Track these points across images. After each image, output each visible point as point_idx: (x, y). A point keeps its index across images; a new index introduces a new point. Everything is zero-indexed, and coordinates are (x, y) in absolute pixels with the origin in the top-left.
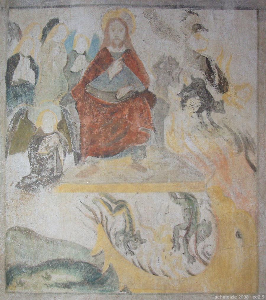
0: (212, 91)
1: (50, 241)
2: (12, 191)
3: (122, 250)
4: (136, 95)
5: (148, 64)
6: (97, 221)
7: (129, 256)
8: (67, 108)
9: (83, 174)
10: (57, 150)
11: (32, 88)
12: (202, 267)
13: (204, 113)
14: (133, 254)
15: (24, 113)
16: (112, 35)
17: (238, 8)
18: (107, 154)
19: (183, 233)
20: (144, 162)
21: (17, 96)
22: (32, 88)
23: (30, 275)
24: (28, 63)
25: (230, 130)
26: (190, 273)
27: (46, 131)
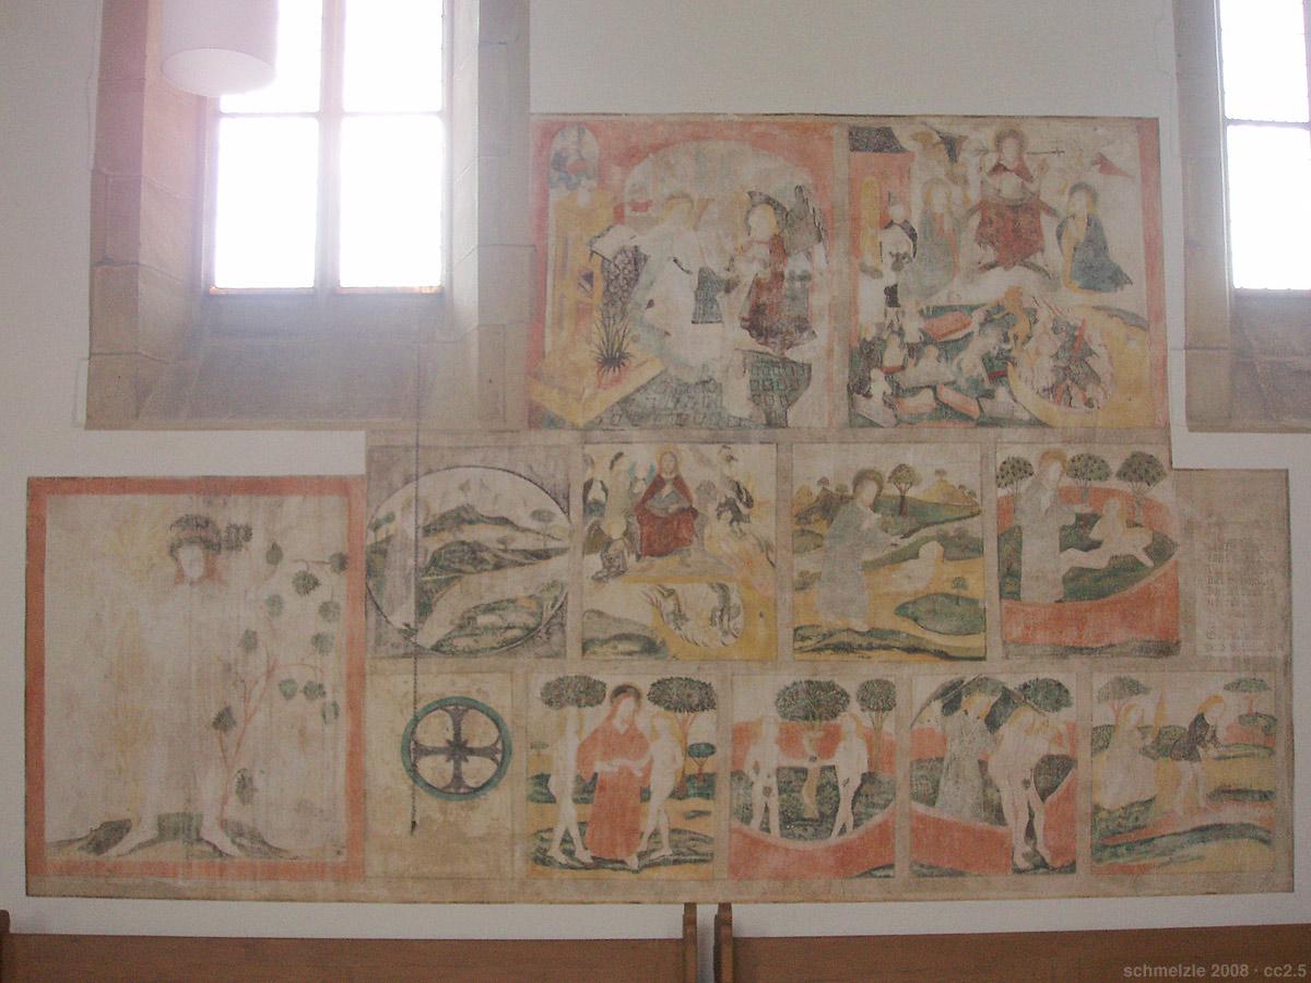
0: (741, 507)
1: (618, 620)
2: (588, 584)
3: (672, 626)
4: (682, 511)
5: (692, 486)
6: (653, 604)
7: (678, 632)
8: (630, 520)
9: (643, 570)
10: (622, 552)
11: (603, 506)
12: (734, 640)
13: (735, 524)
14: (680, 629)
15: (597, 524)
16: (665, 465)
17: (761, 443)
18: (661, 555)
19: (719, 613)
20: (689, 560)
21: (592, 511)
22: (603, 506)
23: (602, 646)
24: (600, 485)
25: (754, 536)
26: (723, 644)
27: (614, 537)
